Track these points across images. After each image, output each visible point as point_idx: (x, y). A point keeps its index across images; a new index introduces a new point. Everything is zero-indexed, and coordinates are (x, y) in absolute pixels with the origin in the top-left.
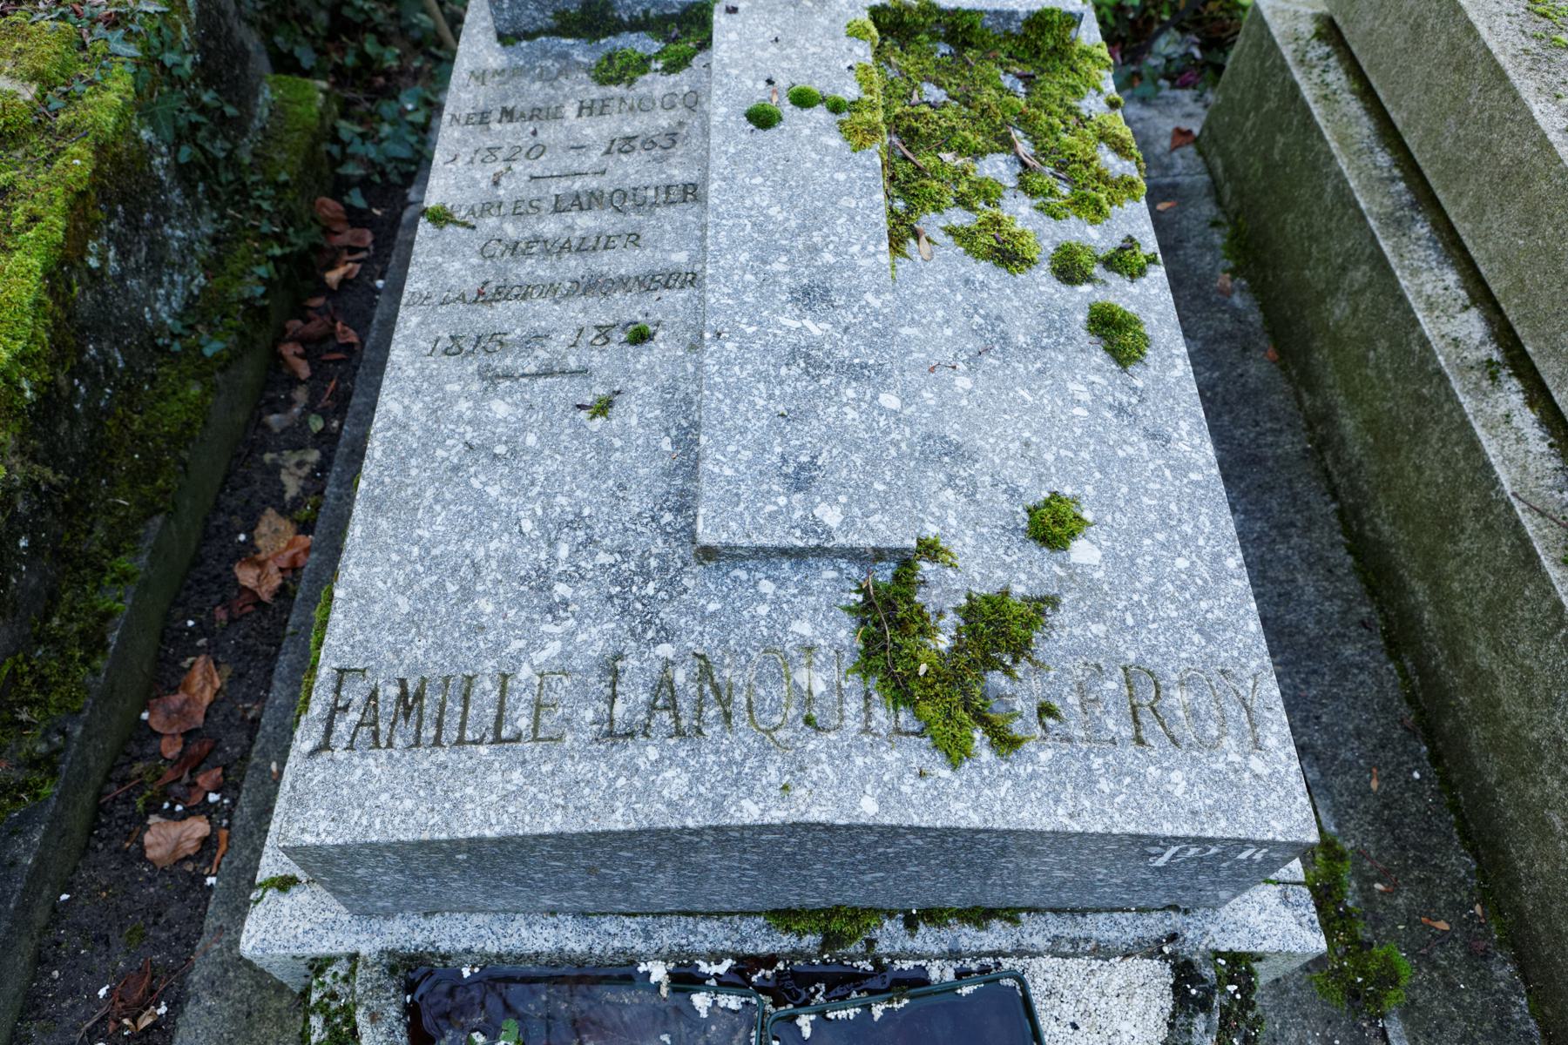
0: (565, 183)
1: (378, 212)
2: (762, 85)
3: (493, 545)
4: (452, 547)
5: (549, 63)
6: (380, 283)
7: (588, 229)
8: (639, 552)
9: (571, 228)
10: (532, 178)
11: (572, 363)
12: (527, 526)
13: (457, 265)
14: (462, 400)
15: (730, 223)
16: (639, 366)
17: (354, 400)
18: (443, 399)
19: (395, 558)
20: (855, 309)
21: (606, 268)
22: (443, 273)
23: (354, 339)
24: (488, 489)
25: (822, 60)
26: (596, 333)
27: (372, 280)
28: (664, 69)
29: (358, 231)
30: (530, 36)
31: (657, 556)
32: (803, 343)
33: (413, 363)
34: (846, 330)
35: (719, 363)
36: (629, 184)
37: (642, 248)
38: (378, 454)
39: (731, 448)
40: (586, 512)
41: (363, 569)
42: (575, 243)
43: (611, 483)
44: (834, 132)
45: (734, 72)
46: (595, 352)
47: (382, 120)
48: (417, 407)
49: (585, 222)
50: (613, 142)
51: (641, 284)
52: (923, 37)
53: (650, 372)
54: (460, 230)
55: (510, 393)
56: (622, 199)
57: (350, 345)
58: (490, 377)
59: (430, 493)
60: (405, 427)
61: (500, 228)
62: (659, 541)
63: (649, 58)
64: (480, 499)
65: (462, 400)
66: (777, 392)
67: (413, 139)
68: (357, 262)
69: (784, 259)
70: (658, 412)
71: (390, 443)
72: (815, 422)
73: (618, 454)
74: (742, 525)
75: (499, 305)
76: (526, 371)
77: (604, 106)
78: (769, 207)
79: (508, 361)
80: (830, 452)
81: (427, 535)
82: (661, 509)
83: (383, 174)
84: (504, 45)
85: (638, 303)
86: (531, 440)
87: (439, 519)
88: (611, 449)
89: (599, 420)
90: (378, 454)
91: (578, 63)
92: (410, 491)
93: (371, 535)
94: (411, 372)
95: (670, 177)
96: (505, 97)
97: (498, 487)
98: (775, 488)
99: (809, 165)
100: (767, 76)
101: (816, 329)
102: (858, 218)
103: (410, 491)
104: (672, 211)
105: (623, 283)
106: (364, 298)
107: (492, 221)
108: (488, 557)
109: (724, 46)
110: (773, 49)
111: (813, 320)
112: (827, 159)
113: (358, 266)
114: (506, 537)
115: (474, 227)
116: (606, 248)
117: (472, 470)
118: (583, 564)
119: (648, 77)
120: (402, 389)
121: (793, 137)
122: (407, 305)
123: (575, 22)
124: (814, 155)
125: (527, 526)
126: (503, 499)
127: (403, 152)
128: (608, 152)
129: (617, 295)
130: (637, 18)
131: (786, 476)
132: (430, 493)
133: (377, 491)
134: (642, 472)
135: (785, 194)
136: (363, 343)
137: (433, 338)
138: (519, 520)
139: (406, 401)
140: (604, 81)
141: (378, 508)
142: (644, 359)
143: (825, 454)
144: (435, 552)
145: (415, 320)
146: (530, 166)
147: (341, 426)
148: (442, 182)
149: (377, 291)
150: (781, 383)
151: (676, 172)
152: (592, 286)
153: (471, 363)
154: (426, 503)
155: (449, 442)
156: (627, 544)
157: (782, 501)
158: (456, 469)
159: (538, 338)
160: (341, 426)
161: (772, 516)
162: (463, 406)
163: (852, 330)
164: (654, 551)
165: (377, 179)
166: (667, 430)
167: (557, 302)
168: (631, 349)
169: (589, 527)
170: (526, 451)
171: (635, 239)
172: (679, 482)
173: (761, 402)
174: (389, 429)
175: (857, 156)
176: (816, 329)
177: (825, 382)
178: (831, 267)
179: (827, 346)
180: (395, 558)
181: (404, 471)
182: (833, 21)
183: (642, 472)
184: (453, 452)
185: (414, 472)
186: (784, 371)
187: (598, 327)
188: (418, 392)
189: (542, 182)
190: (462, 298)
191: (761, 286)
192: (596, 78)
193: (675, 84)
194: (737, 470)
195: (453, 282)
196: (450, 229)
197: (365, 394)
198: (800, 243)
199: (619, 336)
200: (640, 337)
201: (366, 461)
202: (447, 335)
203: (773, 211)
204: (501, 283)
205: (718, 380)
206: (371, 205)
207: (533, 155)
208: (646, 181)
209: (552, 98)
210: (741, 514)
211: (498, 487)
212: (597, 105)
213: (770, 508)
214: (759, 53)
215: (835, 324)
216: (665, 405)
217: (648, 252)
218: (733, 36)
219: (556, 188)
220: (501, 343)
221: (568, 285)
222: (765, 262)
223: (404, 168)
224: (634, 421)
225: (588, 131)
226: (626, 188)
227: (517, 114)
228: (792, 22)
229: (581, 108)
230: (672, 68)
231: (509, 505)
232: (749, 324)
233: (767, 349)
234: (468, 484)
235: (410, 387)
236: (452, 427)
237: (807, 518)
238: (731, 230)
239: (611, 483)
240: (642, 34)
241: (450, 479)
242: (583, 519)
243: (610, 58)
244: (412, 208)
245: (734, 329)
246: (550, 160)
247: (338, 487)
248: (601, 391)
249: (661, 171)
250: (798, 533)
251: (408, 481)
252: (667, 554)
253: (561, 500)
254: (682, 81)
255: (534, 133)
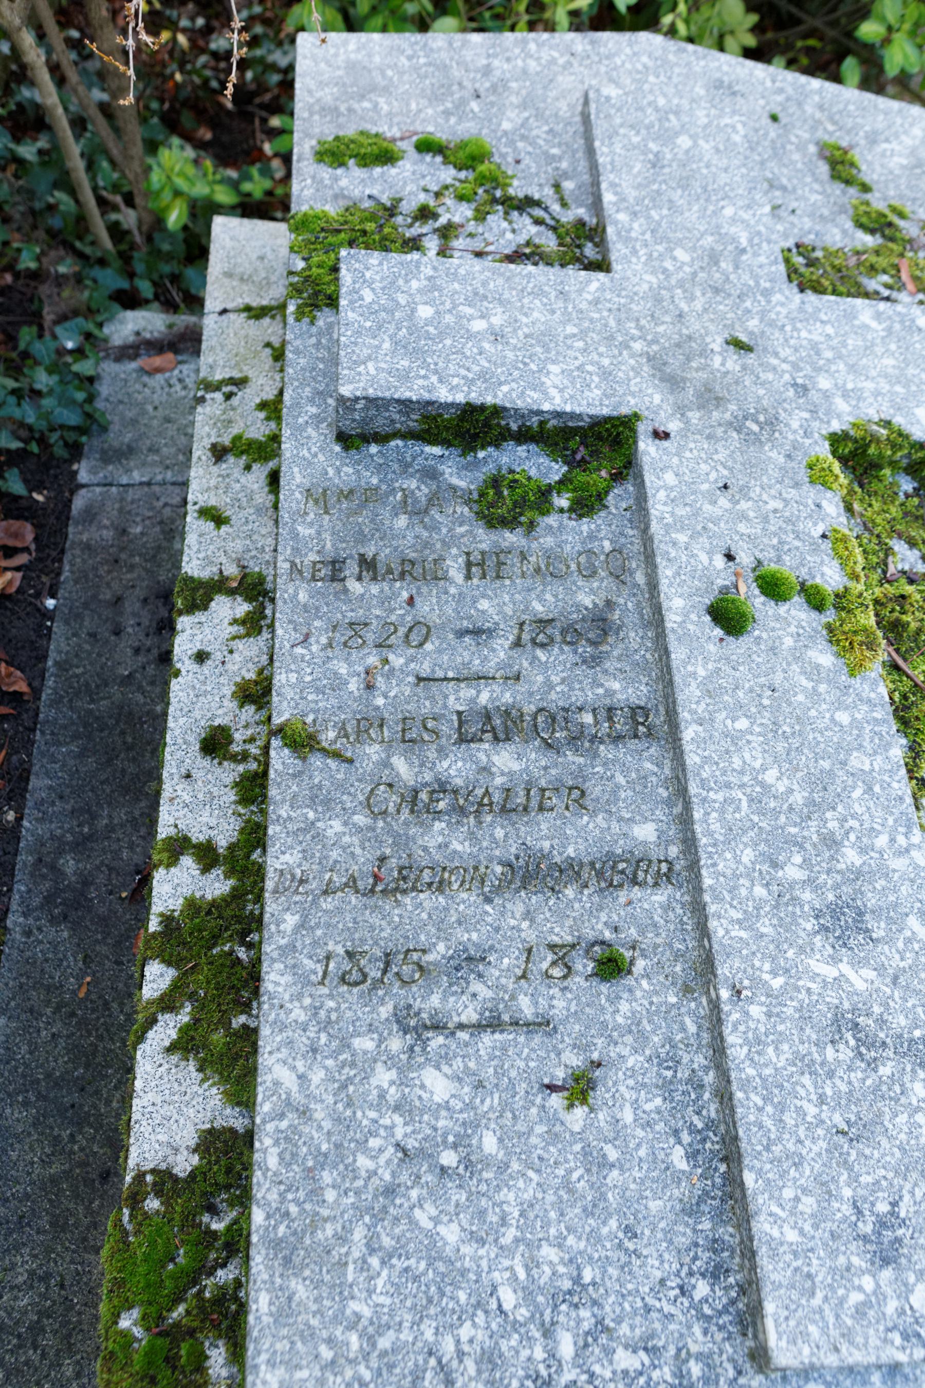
0: (467, 692)
1: (39, 498)
2: (720, 562)
3: (466, 1332)
4: (406, 1336)
5: (413, 484)
6: (50, 603)
7: (511, 774)
8: (672, 1351)
9: (485, 770)
10: (420, 679)
11: (526, 1007)
12: (508, 1298)
13: (337, 826)
14: (380, 1067)
15: (720, 797)
16: (620, 1020)
17: (34, 782)
18: (353, 1065)
19: (326, 1353)
20: (900, 945)
21: (546, 845)
22: (318, 837)
23: (22, 687)
24: (442, 1229)
25: (788, 521)
26: (550, 957)
27: (38, 595)
28: (571, 510)
29: (15, 525)
30: (381, 439)
31: (699, 1357)
32: (846, 1005)
33: (299, 997)
34: (895, 979)
35: (747, 1042)
36: (555, 699)
37: (593, 814)
38: (273, 1162)
39: (788, 1193)
40: (588, 1275)
41: (281, 1372)
42: (497, 797)
43: (613, 1223)
44: (822, 644)
45: (682, 538)
46: (555, 991)
47: (37, 363)
48: (317, 1077)
49: (507, 761)
50: (522, 624)
51: (600, 874)
52: (887, 472)
53: (634, 1028)
54: (332, 763)
55: (447, 1058)
56: (550, 727)
57: (17, 695)
58: (419, 1028)
59: (359, 1234)
60: (304, 1113)
61: (386, 764)
62: (697, 1330)
63: (550, 489)
64: (433, 1251)
65: (380, 1067)
66: (829, 1092)
67: (80, 396)
68: (17, 569)
69: (798, 859)
70: (658, 1101)
71: (287, 1139)
72: (884, 1142)
73: (615, 1173)
74: (825, 1330)
75: (407, 900)
76: (464, 1019)
77: (500, 564)
78: (764, 769)
79: (435, 1000)
80: (912, 1193)
81: (367, 1312)
82: (691, 1274)
83: (42, 441)
84: (346, 448)
85: (600, 909)
86: (490, 1143)
87: (380, 1282)
88: (604, 1164)
89: (580, 1112)
90: (273, 1162)
91: (454, 488)
92: (329, 1230)
93: (285, 1311)
94: (299, 1014)
95: (610, 693)
96: (362, 538)
97: (454, 1226)
98: (855, 1260)
99: (801, 698)
100: (723, 545)
101: (860, 979)
102: (877, 789)
103: (329, 1230)
104: (620, 752)
105: (570, 871)
106: (31, 622)
107: (373, 751)
108: (461, 1355)
109: (662, 495)
110: (724, 502)
111: (852, 965)
112: (822, 688)
113: (19, 575)
114: (480, 1318)
115: (350, 761)
116: (541, 809)
117: (414, 1194)
118: (597, 1369)
119: (552, 520)
120: (290, 1043)
121: (772, 649)
122: (275, 891)
123: (447, 429)
124: (805, 682)
125: (508, 1298)
126: (466, 1250)
127: (72, 418)
128: (518, 644)
129: (570, 892)
130: (530, 428)
131: (865, 1239)
132: (359, 1234)
133: (282, 1230)
134: (655, 1206)
135: (781, 746)
136: (36, 693)
137: (322, 954)
138: (494, 1288)
139: (300, 1065)
140: (493, 522)
141: (287, 1261)
142: (624, 1007)
143: (907, 1198)
144: (384, 1343)
145: (291, 920)
146: (412, 659)
147: (19, 819)
148: (293, 677)
149: (49, 615)
150: (831, 1074)
151: (616, 686)
152: (532, 874)
153: (382, 1002)
154: (356, 1254)
155: (374, 1143)
156: (652, 1336)
157: (868, 1283)
158: (390, 1191)
159: (470, 962)
160: (19, 819)
161: (860, 1312)
162: (384, 1077)
163: (902, 980)
164: (694, 1348)
165: (34, 448)
166: (676, 1132)
167: (488, 900)
168: (604, 988)
169: (595, 1303)
170: (486, 1162)
171: (578, 796)
172: (706, 1225)
173: (812, 1110)
174: (282, 1116)
175: (856, 682)
176: (860, 979)
177: (885, 1070)
178: (858, 874)
179: (877, 1009)
180: (326, 1353)
181: (316, 1193)
182: (789, 456)
183: (655, 1206)
184: (382, 1160)
185: (330, 1195)
186: (830, 1052)
187: (552, 947)
188: (314, 1051)
189: (434, 687)
190: (352, 883)
191: (777, 907)
192: (480, 515)
193: (591, 537)
194: (802, 1232)
195: (334, 854)
196: (316, 761)
197: (47, 774)
198: (812, 831)
199: (584, 965)
200: (611, 967)
201: (258, 1175)
202: (340, 950)
203: (770, 776)
204: (404, 862)
205: (751, 1072)
206: (30, 491)
207: (415, 638)
208: (577, 698)
209: (426, 545)
210: (821, 1311)
211: (454, 1226)
212: (491, 562)
213: (855, 1298)
214: (707, 507)
215: (880, 969)
216: (667, 1088)
217: (600, 818)
218: (670, 478)
219: (458, 698)
220: (421, 968)
221: (499, 869)
222: (775, 865)
223: (71, 437)
224: (628, 1116)
225: (484, 604)
226: (553, 708)
227: (382, 569)
228: (738, 456)
229: (469, 565)
230: (586, 505)
231: (477, 1259)
232: (774, 973)
233: (804, 1017)
234: (413, 1222)
235: (302, 1042)
236: (373, 1114)
237: (903, 1312)
238: (722, 811)
239: (613, 1223)
240: (533, 447)
241: (384, 1210)
242: (584, 1287)
243: (495, 482)
244: (83, 492)
245: (757, 982)
246: (439, 651)
247: (25, 915)
248: (575, 1060)
249: (596, 684)
250: (897, 1339)
251: (325, 1212)
252: (710, 1355)
253: (548, 1253)
254: (602, 530)
255: (411, 601)
